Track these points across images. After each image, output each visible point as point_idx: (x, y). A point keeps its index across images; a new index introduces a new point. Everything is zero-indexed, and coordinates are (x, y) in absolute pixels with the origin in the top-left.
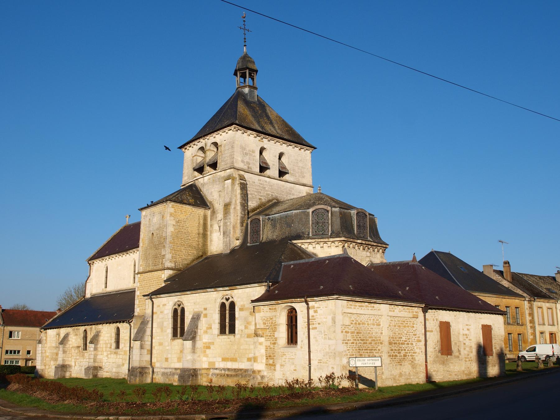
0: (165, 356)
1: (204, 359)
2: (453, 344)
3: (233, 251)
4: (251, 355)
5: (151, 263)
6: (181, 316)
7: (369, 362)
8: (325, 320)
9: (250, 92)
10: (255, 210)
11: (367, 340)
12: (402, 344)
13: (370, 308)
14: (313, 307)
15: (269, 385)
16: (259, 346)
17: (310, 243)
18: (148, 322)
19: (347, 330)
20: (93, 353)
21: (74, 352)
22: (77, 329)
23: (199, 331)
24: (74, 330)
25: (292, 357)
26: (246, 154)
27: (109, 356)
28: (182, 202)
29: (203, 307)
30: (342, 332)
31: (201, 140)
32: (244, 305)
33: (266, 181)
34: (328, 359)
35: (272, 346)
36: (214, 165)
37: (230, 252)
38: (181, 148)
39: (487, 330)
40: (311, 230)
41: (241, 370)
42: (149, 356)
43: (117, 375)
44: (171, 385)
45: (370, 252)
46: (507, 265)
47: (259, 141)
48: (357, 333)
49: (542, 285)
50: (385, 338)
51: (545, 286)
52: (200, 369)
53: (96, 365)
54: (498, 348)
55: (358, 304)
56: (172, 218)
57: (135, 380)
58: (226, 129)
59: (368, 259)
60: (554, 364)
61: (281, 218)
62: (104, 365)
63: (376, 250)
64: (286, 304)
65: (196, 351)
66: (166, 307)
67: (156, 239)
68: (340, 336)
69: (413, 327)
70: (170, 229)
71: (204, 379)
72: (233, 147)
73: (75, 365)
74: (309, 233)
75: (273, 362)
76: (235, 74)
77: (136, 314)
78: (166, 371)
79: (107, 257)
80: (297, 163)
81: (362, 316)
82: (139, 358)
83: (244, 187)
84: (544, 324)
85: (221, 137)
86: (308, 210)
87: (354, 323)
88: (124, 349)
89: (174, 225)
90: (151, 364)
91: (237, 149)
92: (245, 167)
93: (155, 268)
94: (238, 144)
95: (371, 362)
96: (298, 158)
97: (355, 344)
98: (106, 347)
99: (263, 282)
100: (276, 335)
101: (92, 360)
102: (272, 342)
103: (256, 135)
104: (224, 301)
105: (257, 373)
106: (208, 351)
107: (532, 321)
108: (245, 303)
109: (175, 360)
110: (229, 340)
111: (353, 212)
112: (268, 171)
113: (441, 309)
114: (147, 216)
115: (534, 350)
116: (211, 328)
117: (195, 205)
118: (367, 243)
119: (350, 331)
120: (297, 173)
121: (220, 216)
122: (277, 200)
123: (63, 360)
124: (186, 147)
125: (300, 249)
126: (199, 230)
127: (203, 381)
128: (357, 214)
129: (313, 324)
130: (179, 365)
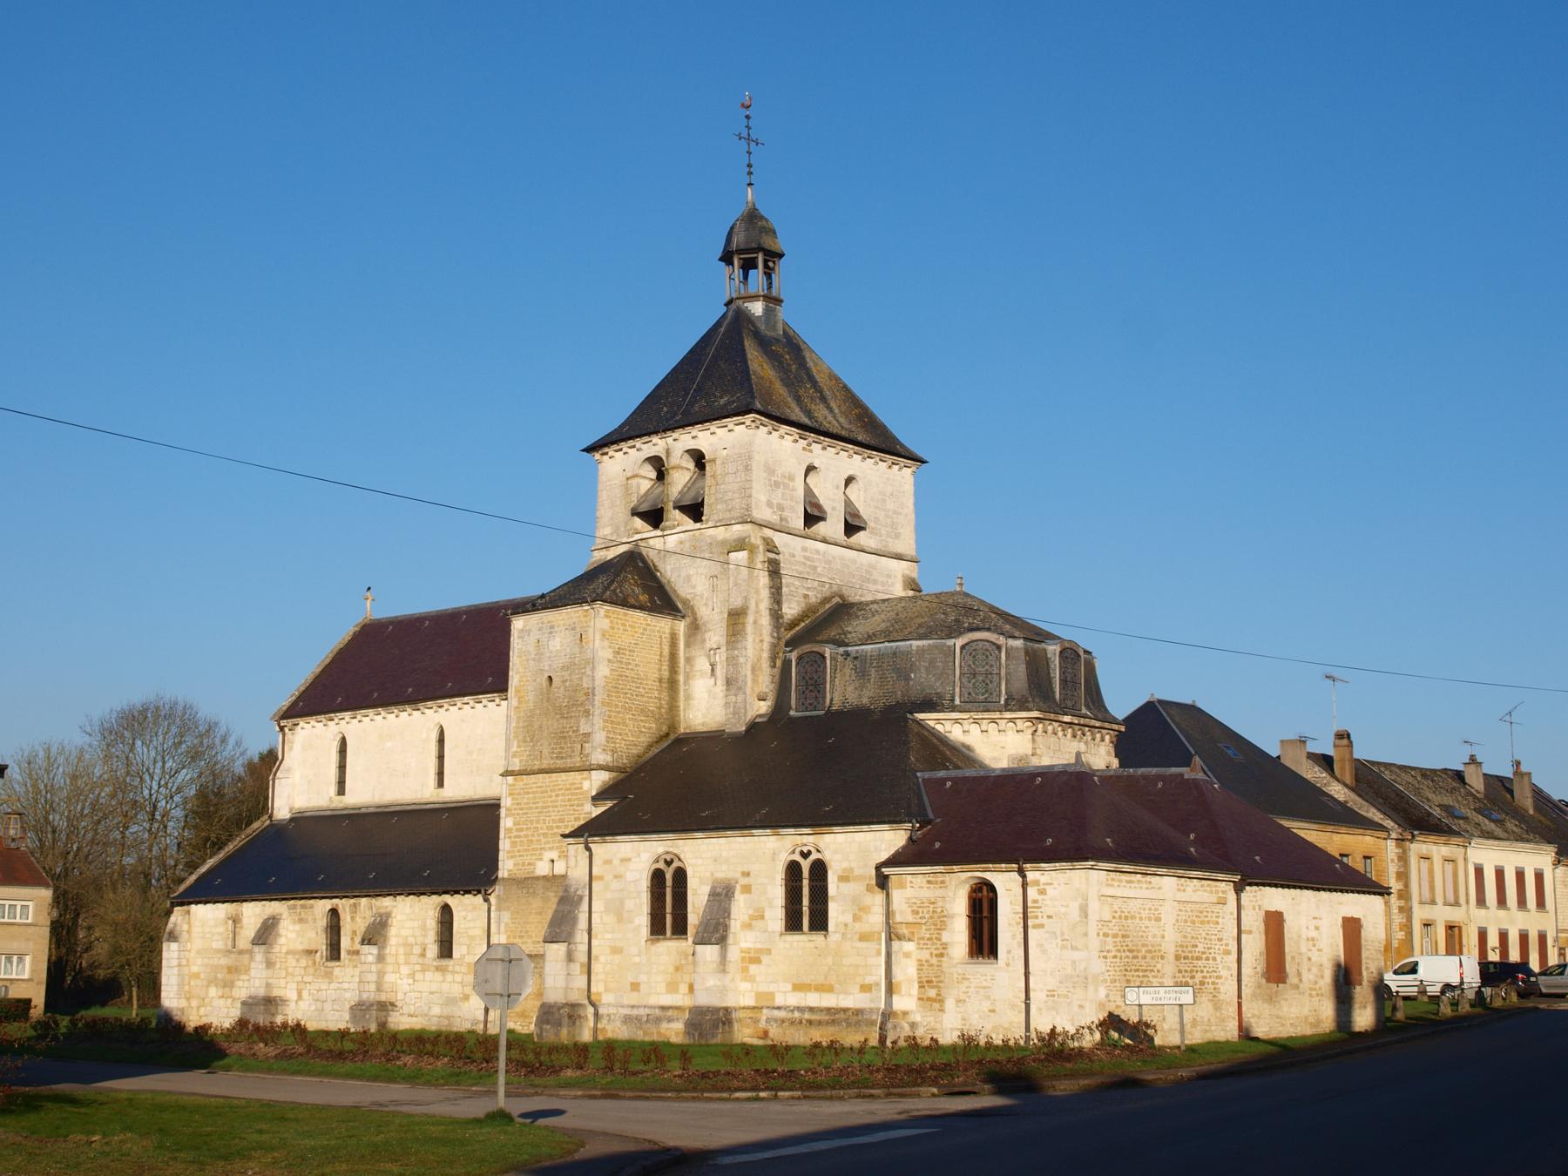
0: (630, 979)
1: (745, 986)
3: (753, 727)
4: (869, 980)
5: (546, 752)
6: (674, 886)
8: (1063, 910)
9: (767, 311)
12: (1198, 958)
14: (1037, 883)
15: (942, 1041)
16: (904, 960)
18: (581, 898)
19: (1106, 930)
20: (374, 968)
21: (296, 965)
22: (303, 907)
24: (289, 908)
26: (777, 484)
27: (419, 976)
29: (740, 869)
31: (655, 439)
32: (851, 870)
33: (818, 552)
35: (934, 961)
37: (748, 730)
38: (590, 449)
39: (1352, 928)
41: (845, 1010)
44: (668, 1044)
46: (1345, 742)
49: (1431, 796)
50: (1169, 948)
51: (1437, 799)
53: (383, 997)
54: (1373, 969)
56: (606, 643)
57: (557, 1034)
60: (1472, 1006)
61: (881, 656)
66: (632, 866)
67: (559, 689)
68: (1094, 942)
70: (603, 671)
71: (747, 1031)
72: (747, 468)
73: (300, 997)
76: (727, 258)
77: (503, 873)
78: (635, 1012)
79: (347, 715)
83: (774, 571)
84: (1433, 902)
85: (710, 438)
86: (950, 642)
90: (589, 997)
91: (758, 475)
92: (774, 519)
93: (560, 764)
94: (755, 458)
96: (882, 485)
98: (408, 954)
100: (945, 937)
101: (373, 987)
104: (797, 857)
106: (753, 969)
108: (853, 865)
109: (662, 987)
110: (812, 945)
111: (1053, 649)
113: (1270, 885)
114: (529, 632)
115: (1413, 969)
116: (762, 917)
118: (1082, 721)
121: (715, 635)
122: (841, 597)
123: (268, 985)
125: (943, 740)
127: (744, 1034)
130: (681, 999)
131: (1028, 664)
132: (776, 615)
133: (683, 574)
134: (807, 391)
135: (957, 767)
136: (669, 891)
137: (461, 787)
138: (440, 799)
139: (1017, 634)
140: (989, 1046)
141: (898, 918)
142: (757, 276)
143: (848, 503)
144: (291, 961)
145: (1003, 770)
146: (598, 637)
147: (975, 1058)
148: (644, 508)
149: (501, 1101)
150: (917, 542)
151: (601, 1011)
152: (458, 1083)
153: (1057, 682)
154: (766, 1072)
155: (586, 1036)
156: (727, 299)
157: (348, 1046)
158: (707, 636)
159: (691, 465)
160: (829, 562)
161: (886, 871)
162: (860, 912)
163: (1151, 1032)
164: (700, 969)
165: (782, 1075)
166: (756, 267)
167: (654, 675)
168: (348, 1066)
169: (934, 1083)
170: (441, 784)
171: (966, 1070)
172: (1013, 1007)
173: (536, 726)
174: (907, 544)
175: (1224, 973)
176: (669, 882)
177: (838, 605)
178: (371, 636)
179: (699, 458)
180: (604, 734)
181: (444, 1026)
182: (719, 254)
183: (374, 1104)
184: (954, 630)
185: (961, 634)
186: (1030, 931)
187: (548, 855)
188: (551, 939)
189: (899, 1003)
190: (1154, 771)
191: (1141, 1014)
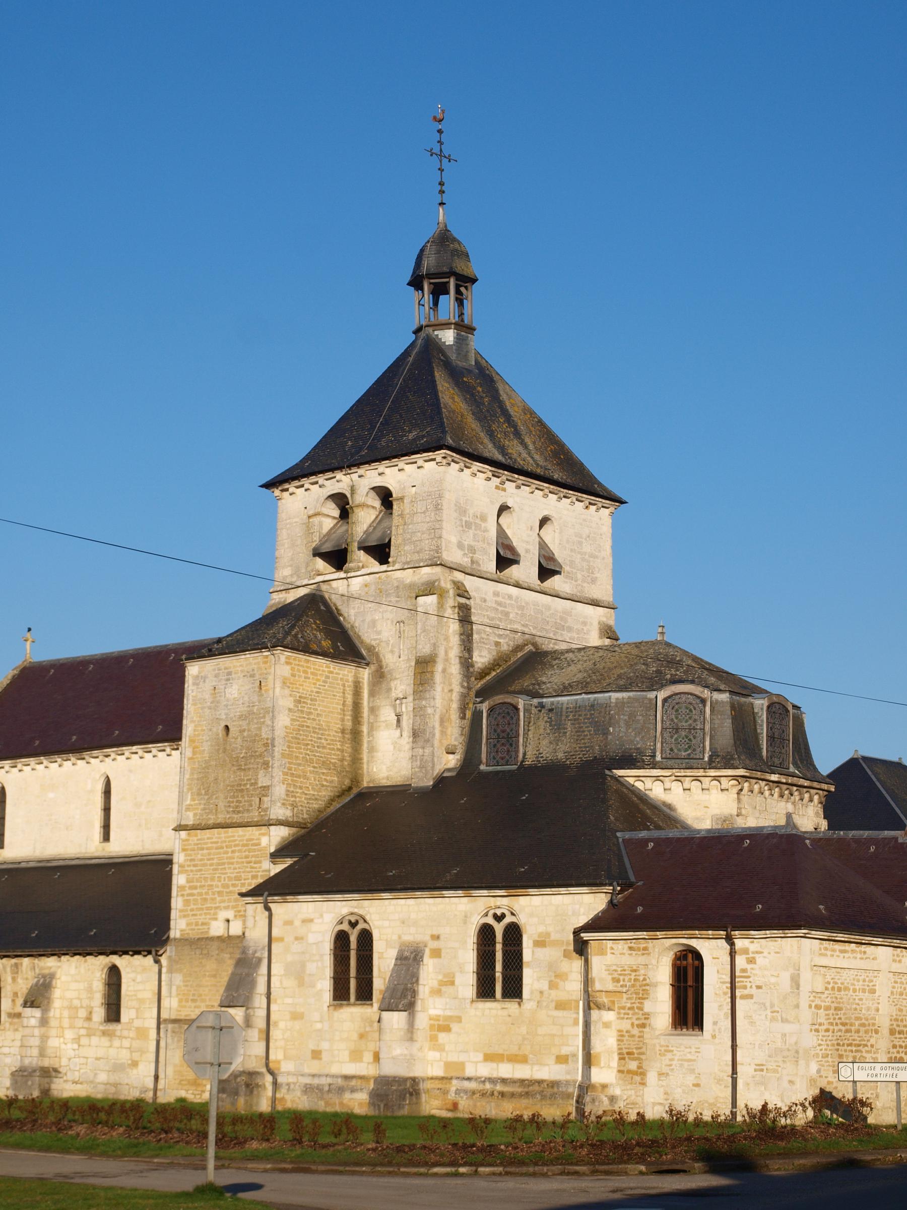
0: (312, 1046)
1: (433, 1055)
3: (441, 781)
4: (565, 1051)
5: (221, 805)
6: (359, 949)
7: (884, 1072)
8: (773, 980)
9: (459, 340)
10: (488, 674)
11: (851, 1025)
13: (859, 956)
14: (746, 951)
16: (603, 1031)
18: (260, 960)
23: (421, 988)
25: (689, 1057)
26: (468, 525)
27: (84, 1041)
29: (429, 932)
30: (810, 1006)
31: (339, 475)
33: (510, 597)
34: (780, 1064)
35: (636, 1031)
37: (435, 785)
38: (270, 485)
40: (659, 745)
41: (540, 1082)
42: (264, 1044)
43: (113, 1090)
45: (794, 803)
47: (497, 487)
48: (836, 1009)
50: (884, 1023)
52: (423, 1080)
53: (46, 1063)
55: (838, 946)
56: (287, 692)
57: (233, 1104)
58: (419, 458)
62: (63, 1063)
63: (807, 796)
64: (674, 941)
66: (314, 927)
67: (236, 740)
68: (806, 1015)
70: (283, 721)
71: (436, 1103)
72: (438, 508)
75: (639, 1067)
76: (416, 283)
78: (316, 1081)
80: (580, 543)
81: (845, 973)
83: (465, 618)
85: (401, 475)
86: (651, 695)
87: (830, 986)
89: (290, 710)
90: (267, 1065)
92: (465, 561)
93: (236, 818)
94: (446, 497)
95: (890, 1072)
96: (580, 528)
97: (830, 1033)
98: (73, 1018)
99: (605, 885)
100: (648, 1006)
101: (35, 1052)
102: (636, 1022)
103: (490, 474)
104: (490, 920)
105: (600, 1089)
106: (442, 1037)
108: (551, 929)
109: (345, 1055)
110: (505, 1013)
111: (760, 704)
112: (514, 567)
116: (452, 983)
117: (335, 655)
119: (823, 1004)
121: (402, 684)
122: (534, 644)
124: (286, 486)
125: (643, 798)
126: (343, 720)
127: (432, 1106)
128: (768, 707)
129: (745, 987)
130: (365, 1068)
131: (734, 719)
132: (466, 663)
133: (368, 618)
134: (500, 426)
135: (658, 828)
137: (127, 842)
138: (106, 854)
139: (722, 687)
140: (698, 1122)
141: (598, 986)
142: (448, 302)
143: (543, 545)
145: (708, 831)
146: (278, 685)
147: (683, 1135)
148: (327, 547)
149: (211, 1174)
152: (136, 1155)
153: (765, 740)
154: (465, 1147)
155: (264, 1106)
156: (415, 326)
157: (16, 1114)
158: (393, 684)
159: (377, 503)
160: (521, 608)
161: (585, 936)
162: (556, 978)
163: (866, 1110)
164: (387, 1037)
165: (482, 1150)
166: (447, 292)
168: (17, 1136)
169: (641, 1160)
170: (106, 837)
171: (674, 1147)
172: (719, 1081)
173: (212, 777)
174: (603, 589)
177: (530, 652)
178: (31, 677)
179: (386, 497)
181: (111, 1093)
182: (408, 277)
183: (58, 1175)
184: (656, 683)
185: (662, 686)
186: (739, 1003)
187: (223, 914)
188: (229, 1002)
189: (598, 1076)
190: (866, 834)
191: (855, 1091)
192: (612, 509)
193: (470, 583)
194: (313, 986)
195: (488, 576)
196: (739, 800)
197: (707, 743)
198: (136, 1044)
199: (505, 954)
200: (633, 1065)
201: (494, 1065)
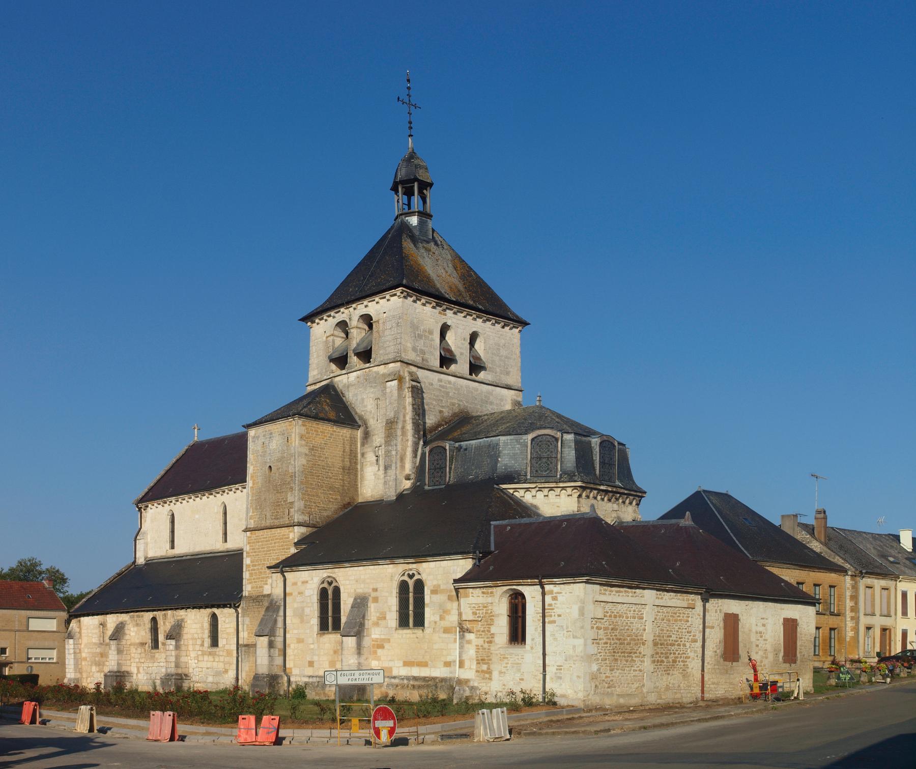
0: (308, 659)
2: (741, 645)
3: (401, 496)
4: (449, 659)
8: (568, 611)
9: (421, 223)
14: (551, 592)
17: (527, 489)
18: (279, 607)
19: (598, 625)
20: (173, 653)
22: (138, 616)
23: (366, 622)
25: (517, 661)
26: (420, 336)
27: (201, 658)
28: (316, 418)
30: (592, 628)
32: (439, 586)
33: (450, 382)
35: (486, 646)
36: (366, 355)
39: (790, 626)
41: (434, 679)
46: (822, 515)
50: (648, 636)
53: (180, 671)
58: (387, 295)
59: (614, 515)
65: (362, 652)
66: (308, 586)
69: (688, 621)
73: (138, 672)
74: (526, 473)
75: (488, 669)
76: (395, 189)
79: (173, 499)
80: (499, 349)
82: (262, 660)
83: (417, 392)
84: (873, 614)
85: (375, 307)
86: (524, 437)
88: (227, 647)
90: (285, 670)
92: (418, 360)
93: (277, 523)
94: (387, 307)
96: (498, 341)
101: (173, 665)
103: (434, 304)
104: (406, 578)
106: (380, 652)
107: (855, 609)
108: (440, 582)
110: (415, 636)
111: (595, 441)
114: (258, 437)
116: (385, 618)
120: (500, 366)
121: (378, 438)
123: (118, 664)
126: (343, 461)
128: (601, 443)
129: (551, 616)
133: (359, 398)
136: (330, 602)
144: (133, 650)
148: (336, 355)
150: (522, 377)
151: (292, 679)
153: (605, 466)
160: (458, 389)
167: (338, 463)
174: (514, 378)
175: (692, 655)
176: (330, 596)
180: (302, 503)
182: (391, 185)
192: (520, 328)
193: (421, 374)
194: (309, 622)
195: (434, 369)
196: (579, 502)
197: (559, 467)
198: (227, 659)
199: (415, 599)
200: (485, 667)
201: (409, 668)
